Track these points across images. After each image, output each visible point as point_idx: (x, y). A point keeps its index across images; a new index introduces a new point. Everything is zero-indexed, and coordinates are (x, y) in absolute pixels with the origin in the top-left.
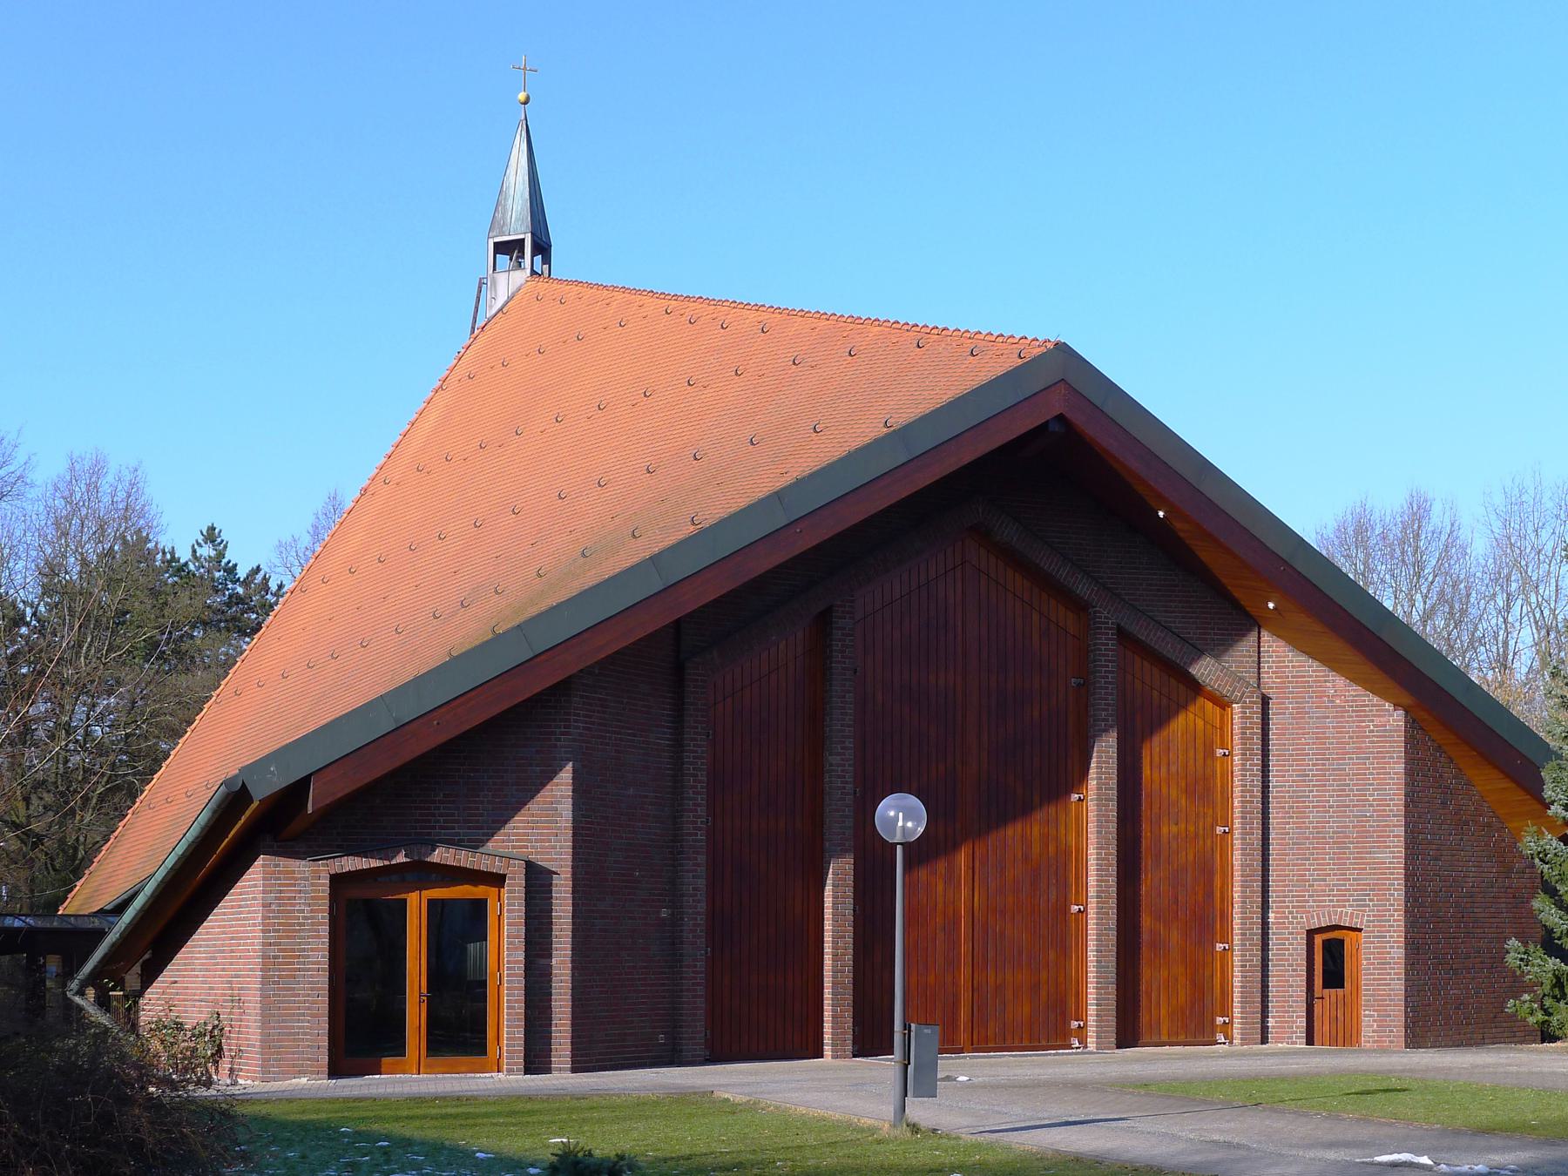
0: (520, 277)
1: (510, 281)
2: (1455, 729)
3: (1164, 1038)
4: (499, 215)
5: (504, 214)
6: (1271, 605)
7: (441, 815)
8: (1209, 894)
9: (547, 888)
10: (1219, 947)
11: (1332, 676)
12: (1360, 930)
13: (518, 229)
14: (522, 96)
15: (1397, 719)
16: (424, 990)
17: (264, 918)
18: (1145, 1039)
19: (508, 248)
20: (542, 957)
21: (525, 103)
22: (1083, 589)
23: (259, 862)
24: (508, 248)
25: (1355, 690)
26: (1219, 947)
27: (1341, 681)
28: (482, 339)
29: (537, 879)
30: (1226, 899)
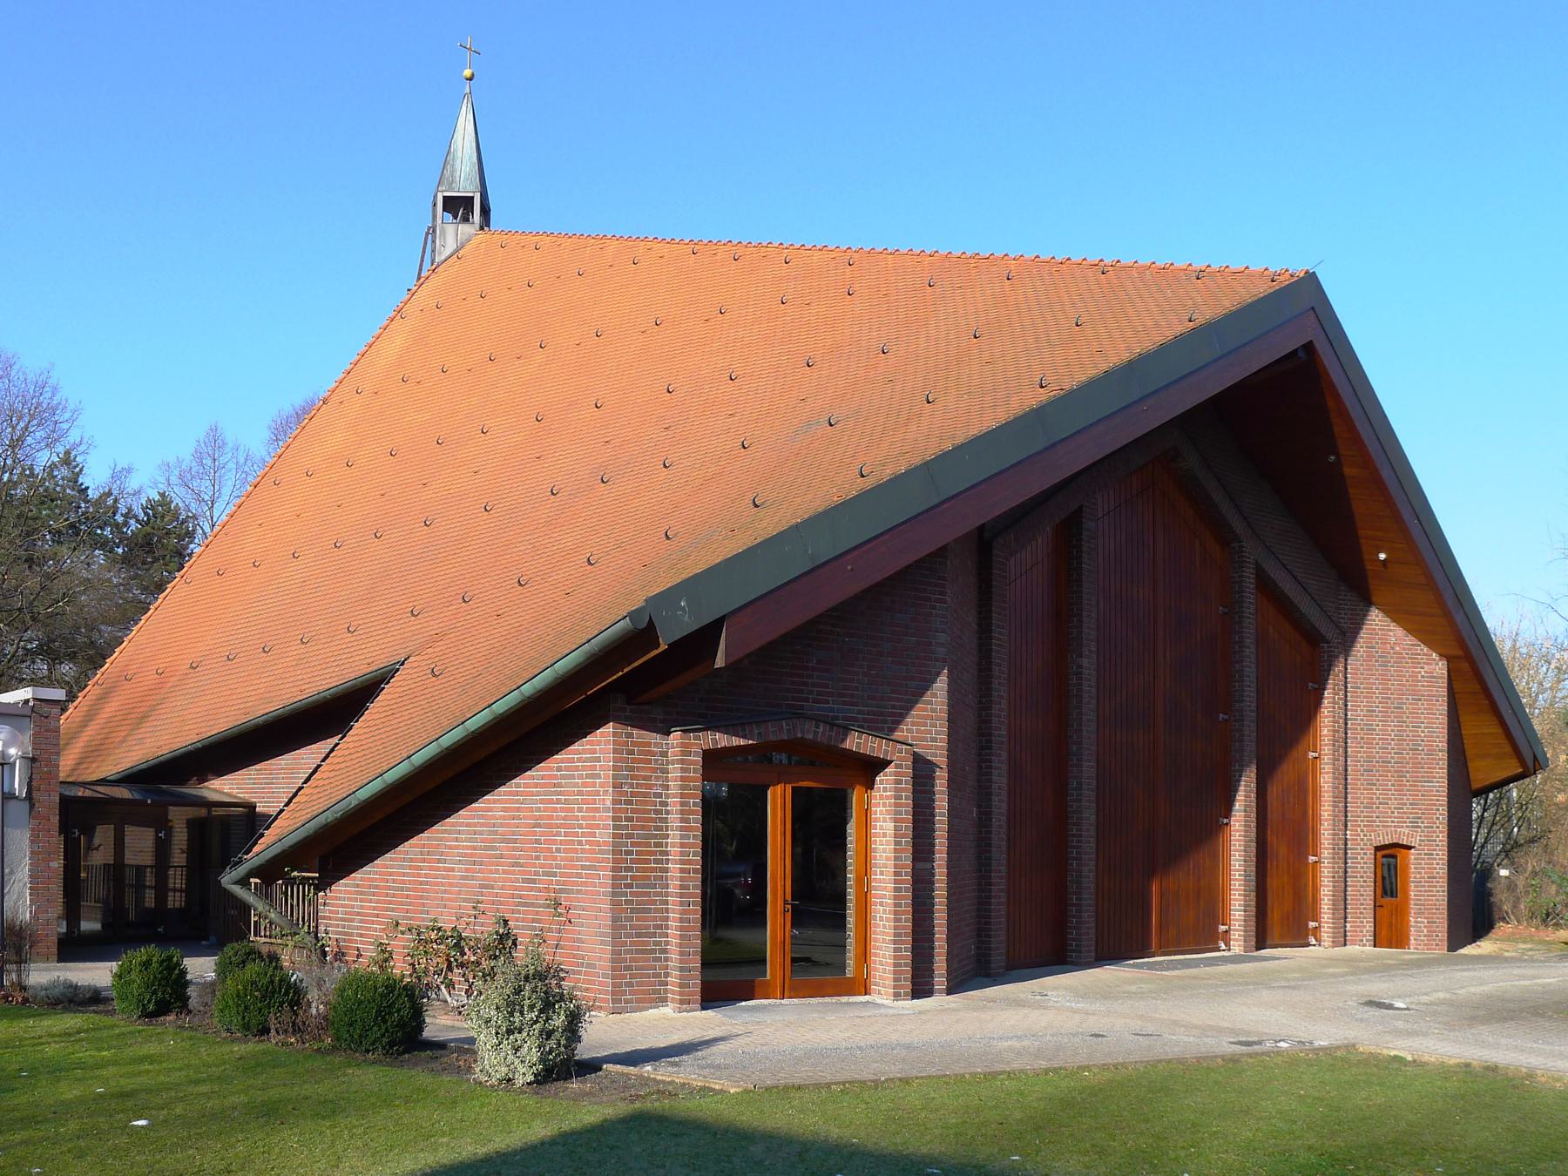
0: (465, 229)
1: (453, 233)
2: (1477, 679)
3: (1277, 942)
4: (447, 173)
5: (453, 172)
6: (1382, 556)
7: (814, 685)
8: (1305, 813)
9: (931, 778)
10: (1312, 859)
11: (1393, 626)
12: (1410, 848)
13: (465, 185)
14: (467, 73)
15: (1440, 668)
16: (789, 897)
17: (615, 802)
18: (1269, 942)
19: (457, 206)
20: (38, 853)
21: (470, 79)
22: (1237, 525)
23: (609, 728)
24: (457, 206)
25: (1410, 640)
26: (1312, 859)
27: (1400, 632)
28: (435, 281)
29: (922, 771)
30: (1316, 818)
